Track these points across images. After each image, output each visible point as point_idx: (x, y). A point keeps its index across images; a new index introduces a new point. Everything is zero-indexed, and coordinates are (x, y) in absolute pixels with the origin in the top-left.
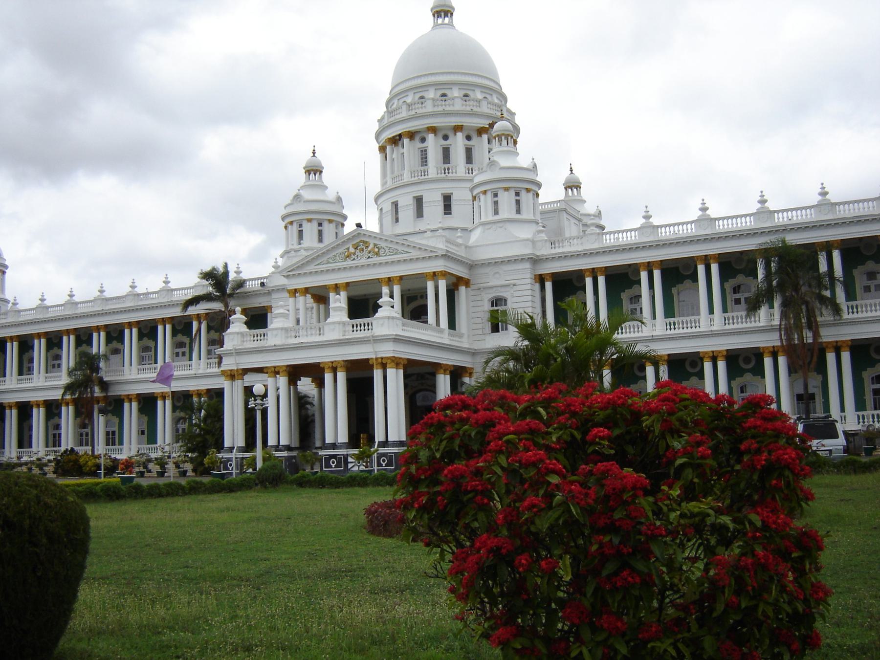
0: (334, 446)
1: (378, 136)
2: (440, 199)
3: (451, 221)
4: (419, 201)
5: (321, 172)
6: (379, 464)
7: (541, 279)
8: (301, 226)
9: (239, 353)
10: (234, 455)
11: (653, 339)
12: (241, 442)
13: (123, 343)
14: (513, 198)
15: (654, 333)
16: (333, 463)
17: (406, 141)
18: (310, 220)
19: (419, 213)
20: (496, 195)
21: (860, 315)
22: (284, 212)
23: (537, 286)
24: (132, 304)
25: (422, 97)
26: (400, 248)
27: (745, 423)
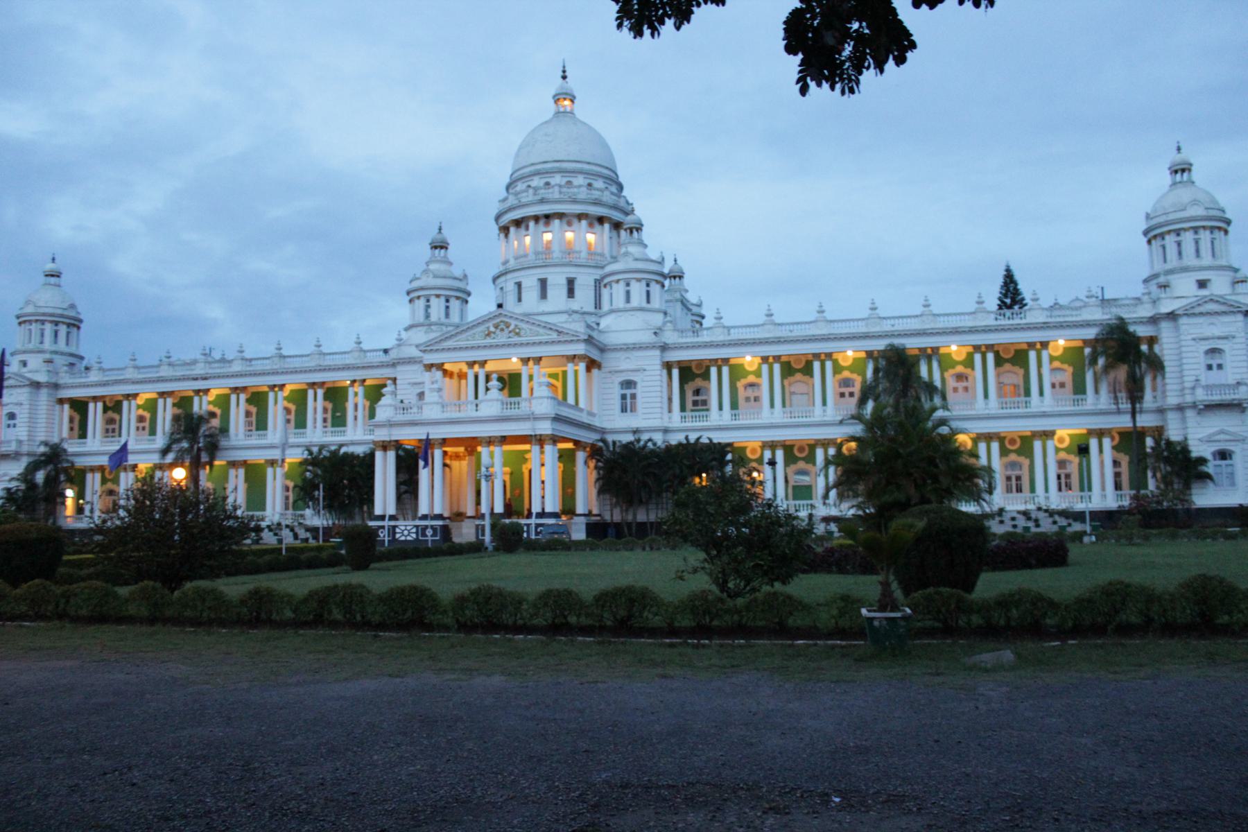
0: (382, 518)
1: (497, 218)
2: (565, 282)
3: (575, 305)
4: (543, 283)
5: (1190, 170)
7: (668, 366)
8: (428, 301)
9: (391, 424)
10: (533, 521)
11: (353, 443)
12: (552, 505)
13: (973, 368)
14: (644, 288)
18: (618, 281)
19: (544, 295)
20: (628, 285)
22: (1144, 227)
23: (665, 372)
24: (96, 379)
26: (542, 331)
27: (263, 520)
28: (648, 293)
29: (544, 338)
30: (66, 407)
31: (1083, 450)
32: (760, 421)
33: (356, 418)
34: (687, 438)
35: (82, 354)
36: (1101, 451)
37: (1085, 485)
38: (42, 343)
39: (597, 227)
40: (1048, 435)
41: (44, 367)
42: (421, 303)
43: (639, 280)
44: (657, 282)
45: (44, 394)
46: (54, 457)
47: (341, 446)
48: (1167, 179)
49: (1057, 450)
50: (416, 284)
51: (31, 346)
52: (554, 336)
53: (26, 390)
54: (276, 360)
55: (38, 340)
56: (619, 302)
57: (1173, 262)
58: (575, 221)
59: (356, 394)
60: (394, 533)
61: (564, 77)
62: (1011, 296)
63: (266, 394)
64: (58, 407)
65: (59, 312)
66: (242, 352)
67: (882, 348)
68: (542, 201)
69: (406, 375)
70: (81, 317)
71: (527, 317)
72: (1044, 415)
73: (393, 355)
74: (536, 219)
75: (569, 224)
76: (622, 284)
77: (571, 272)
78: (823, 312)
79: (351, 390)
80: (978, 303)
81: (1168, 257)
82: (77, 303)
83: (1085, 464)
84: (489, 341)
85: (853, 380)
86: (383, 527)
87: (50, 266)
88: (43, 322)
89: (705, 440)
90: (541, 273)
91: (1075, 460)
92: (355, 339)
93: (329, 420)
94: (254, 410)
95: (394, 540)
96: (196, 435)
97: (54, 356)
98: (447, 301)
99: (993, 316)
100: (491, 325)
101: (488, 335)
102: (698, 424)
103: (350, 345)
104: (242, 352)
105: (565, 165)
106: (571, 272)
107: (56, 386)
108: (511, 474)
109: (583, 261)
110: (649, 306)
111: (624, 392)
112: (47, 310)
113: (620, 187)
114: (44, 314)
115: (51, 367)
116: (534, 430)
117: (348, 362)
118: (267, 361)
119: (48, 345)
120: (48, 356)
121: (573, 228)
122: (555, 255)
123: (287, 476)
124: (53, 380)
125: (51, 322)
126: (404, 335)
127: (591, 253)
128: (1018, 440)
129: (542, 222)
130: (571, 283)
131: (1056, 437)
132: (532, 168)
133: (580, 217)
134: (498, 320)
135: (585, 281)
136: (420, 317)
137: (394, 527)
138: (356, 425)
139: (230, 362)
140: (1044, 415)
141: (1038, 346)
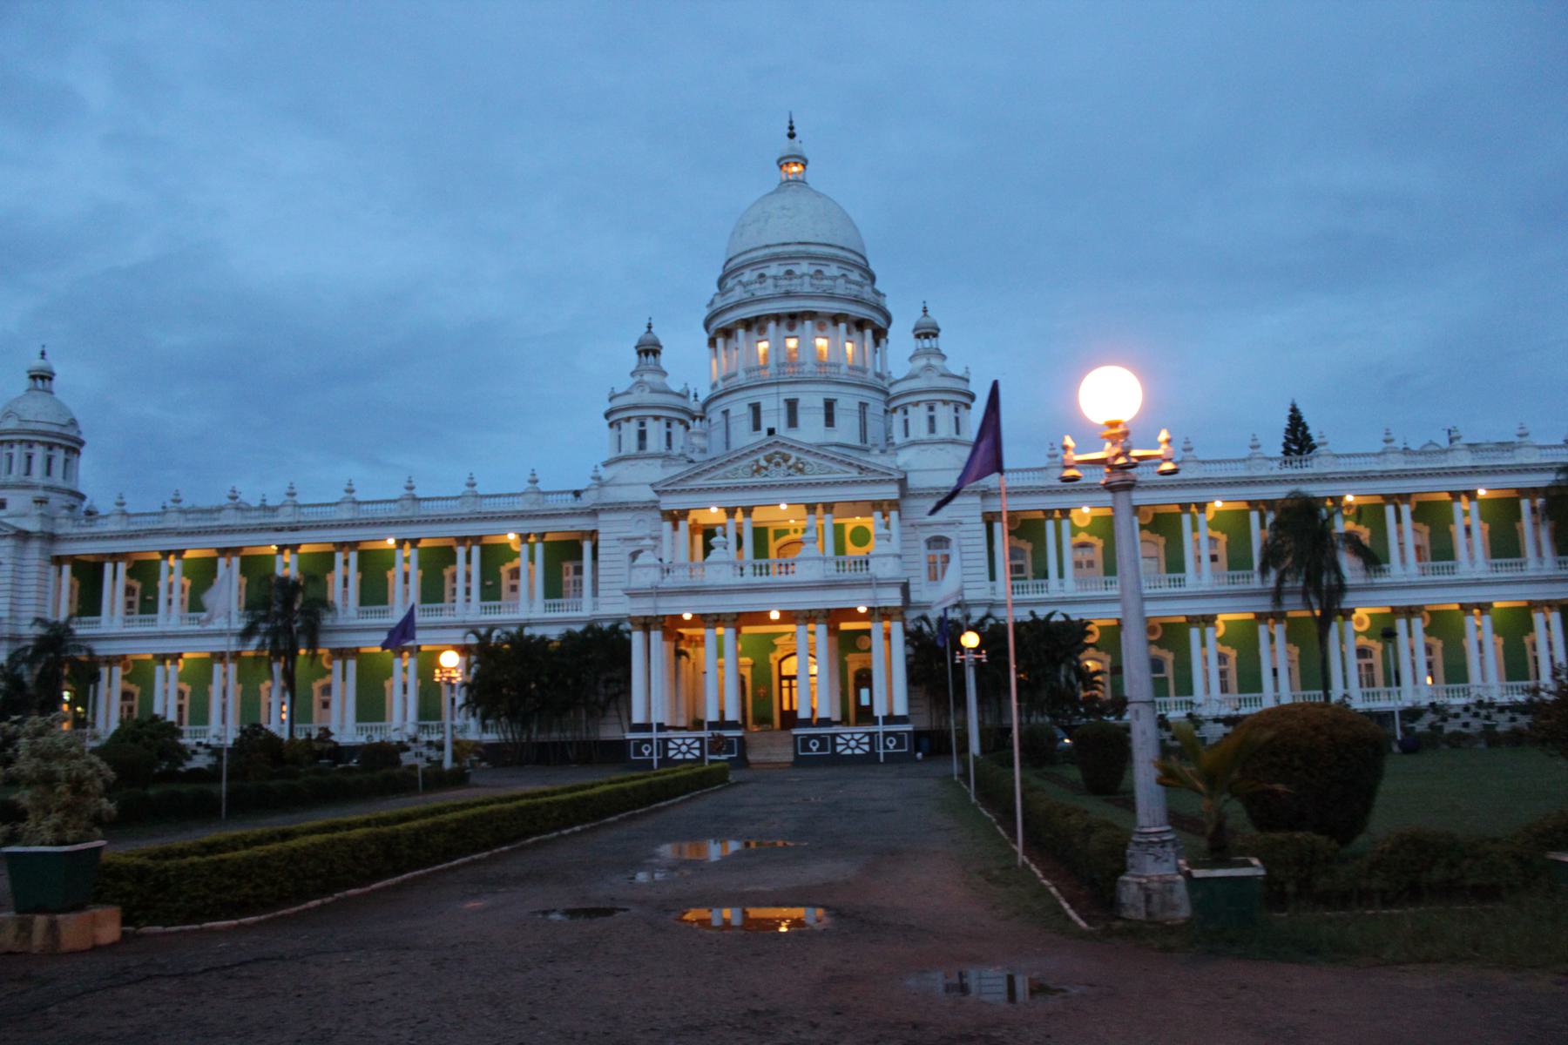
0: (646, 727)
1: (707, 326)
2: (821, 404)
6: (886, 747)
8: (642, 424)
14: (664, 430)
15: (532, 616)
16: (814, 747)
17: (741, 332)
18: (657, 418)
21: (1026, 596)
22: (608, 406)
23: (983, 527)
24: (118, 528)
25: (762, 276)
26: (836, 467)
28: (669, 435)
29: (842, 477)
30: (67, 569)
31: (1389, 635)
32: (1045, 595)
33: (170, 602)
34: (1032, 613)
35: (82, 490)
36: (1410, 634)
37: (1393, 678)
38: (28, 473)
39: (856, 335)
40: (1209, 620)
41: (36, 511)
42: (630, 430)
43: (945, 402)
44: (682, 422)
45: (34, 550)
46: (55, 640)
47: (522, 626)
48: (26, 382)
49: (1357, 634)
50: (618, 402)
51: (12, 478)
52: (854, 474)
53: (9, 542)
54: (407, 503)
55: (23, 470)
56: (919, 429)
57: (16, 475)
58: (829, 325)
59: (171, 570)
60: (666, 749)
61: (792, 136)
62: (1298, 439)
63: (156, 564)
64: (53, 569)
65: (56, 429)
66: (411, 488)
67: (1283, 496)
68: (788, 295)
69: (611, 529)
70: (83, 437)
71: (818, 450)
72: (1478, 583)
73: (587, 500)
74: (777, 318)
75: (821, 327)
76: (923, 408)
77: (788, 392)
78: (473, 485)
79: (279, 558)
80: (347, 491)
81: (14, 469)
82: (78, 417)
83: (1391, 652)
84: (758, 479)
85: (1023, 551)
86: (650, 741)
87: (37, 363)
88: (30, 444)
89: (1058, 618)
90: (788, 392)
91: (1376, 646)
92: (466, 480)
93: (137, 605)
94: (137, 585)
95: (666, 761)
96: (286, 615)
97: (50, 494)
98: (931, 409)
99: (1276, 464)
100: (761, 457)
101: (758, 471)
102: (431, 619)
103: (524, 485)
104: (351, 491)
105: (813, 249)
106: (831, 391)
107: (52, 538)
108: (753, 666)
109: (844, 378)
110: (935, 437)
111: (931, 552)
112: (32, 426)
113: (873, 278)
114: (34, 432)
115: (44, 510)
116: (656, 608)
117: (519, 508)
118: (392, 506)
119: (37, 475)
120: (41, 493)
121: (795, 333)
122: (807, 368)
123: (182, 678)
124: (47, 529)
125: (43, 443)
126: (606, 474)
127: (821, 364)
128: (1160, 630)
129: (783, 325)
130: (829, 405)
131: (1354, 617)
132: (767, 251)
133: (836, 319)
134: (772, 451)
135: (847, 402)
136: (630, 444)
137: (666, 741)
138: (169, 611)
139: (274, 509)
140: (1478, 583)
141: (1057, 515)
